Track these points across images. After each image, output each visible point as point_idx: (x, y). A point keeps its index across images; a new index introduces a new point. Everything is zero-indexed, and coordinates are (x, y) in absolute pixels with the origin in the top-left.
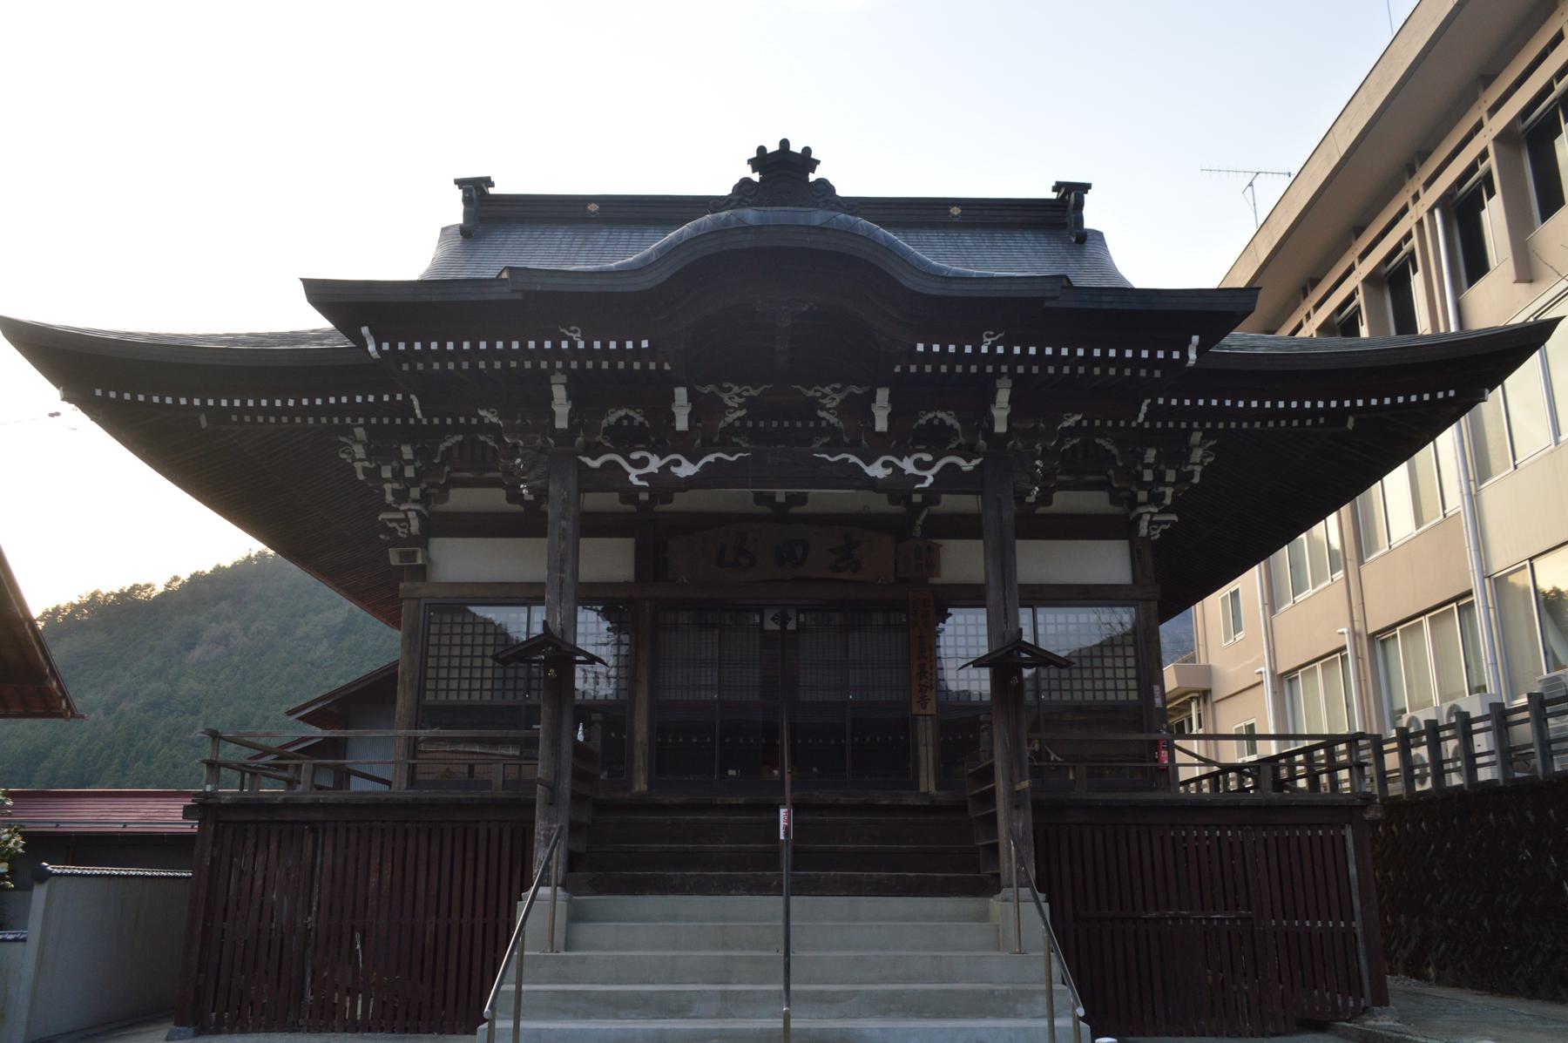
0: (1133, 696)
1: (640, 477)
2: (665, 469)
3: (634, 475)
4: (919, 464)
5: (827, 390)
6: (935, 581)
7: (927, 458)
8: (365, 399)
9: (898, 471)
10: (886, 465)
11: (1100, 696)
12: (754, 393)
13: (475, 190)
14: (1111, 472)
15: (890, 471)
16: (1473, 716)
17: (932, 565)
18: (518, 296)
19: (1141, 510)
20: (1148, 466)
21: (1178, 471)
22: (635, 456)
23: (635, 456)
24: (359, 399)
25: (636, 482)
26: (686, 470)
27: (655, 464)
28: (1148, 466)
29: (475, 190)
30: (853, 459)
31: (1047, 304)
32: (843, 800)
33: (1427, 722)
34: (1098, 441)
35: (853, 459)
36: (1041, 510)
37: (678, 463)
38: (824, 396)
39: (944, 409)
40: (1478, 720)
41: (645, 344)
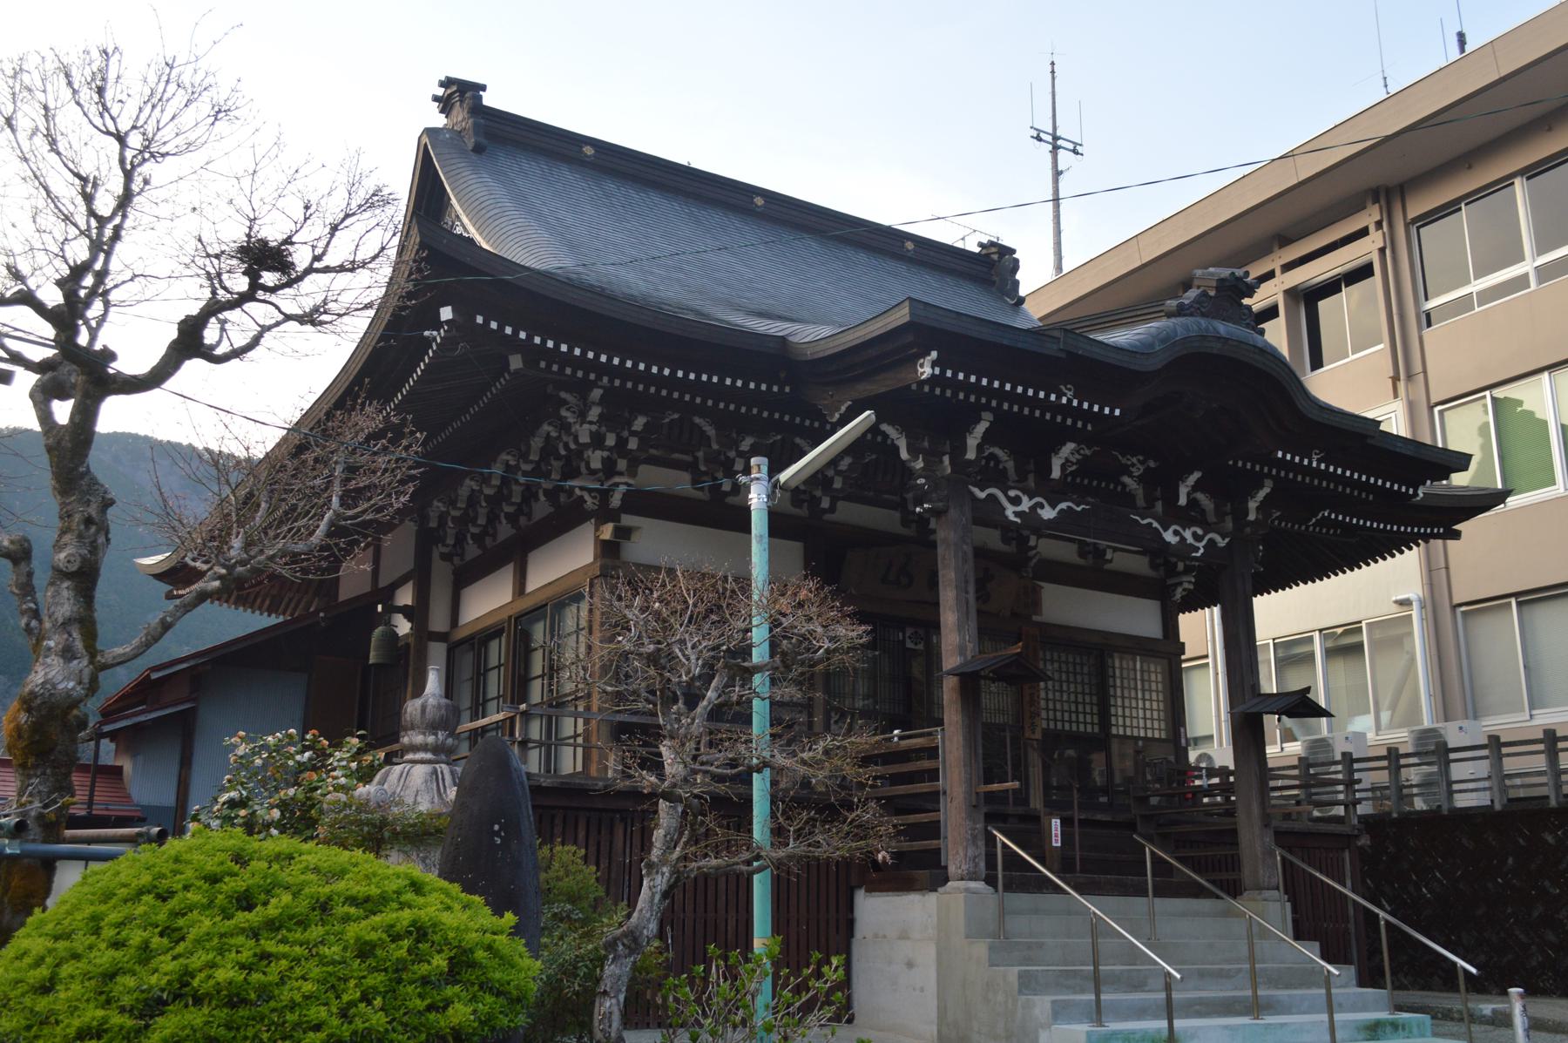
0: (1096, 729)
1: (1016, 514)
2: (1033, 508)
3: (1010, 511)
4: (1195, 535)
5: (1134, 460)
6: (1035, 618)
7: (1200, 532)
8: (710, 378)
9: (1183, 539)
10: (1176, 533)
11: (1074, 728)
12: (1088, 452)
13: (459, 93)
14: (700, 454)
15: (1177, 539)
16: (1401, 751)
17: (1036, 605)
18: (1063, 355)
19: (617, 479)
20: (634, 434)
21: (618, 436)
22: (1012, 493)
23: (1012, 493)
24: (739, 383)
25: (1012, 518)
26: (1048, 513)
27: (1026, 504)
28: (634, 434)
29: (459, 93)
30: (1156, 525)
31: (1369, 441)
32: (85, 846)
33: (1344, 754)
34: (697, 420)
35: (1156, 525)
36: (827, 517)
37: (1042, 507)
38: (1133, 465)
39: (1002, 448)
40: (1407, 755)
41: (1117, 412)
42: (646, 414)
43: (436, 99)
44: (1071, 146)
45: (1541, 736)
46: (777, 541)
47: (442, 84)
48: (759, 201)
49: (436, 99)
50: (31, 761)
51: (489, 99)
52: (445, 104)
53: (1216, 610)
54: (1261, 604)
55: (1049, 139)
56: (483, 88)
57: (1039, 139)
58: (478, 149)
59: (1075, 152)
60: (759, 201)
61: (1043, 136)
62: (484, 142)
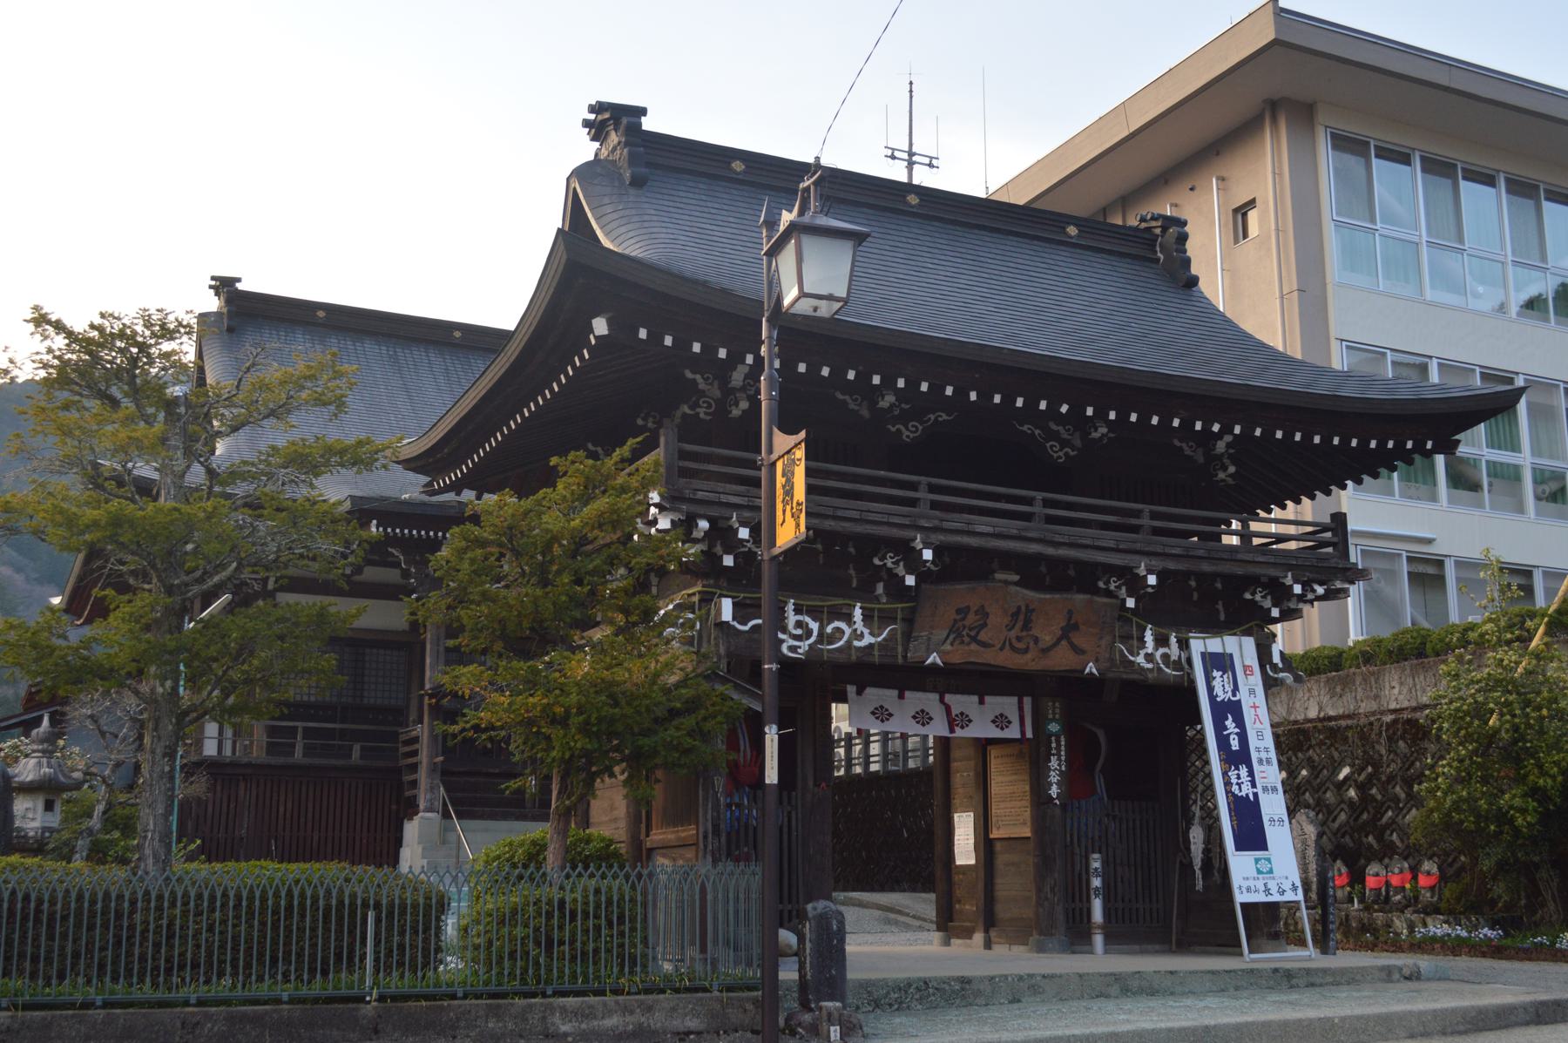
13: (612, 120)
29: (612, 120)
42: (791, 552)
43: (586, 123)
44: (927, 161)
45: (1327, 520)
46: (1429, 176)
47: (592, 109)
48: (321, 314)
49: (586, 123)
50: (1338, 689)
51: (648, 124)
52: (597, 130)
53: (973, 862)
54: (959, 862)
55: (905, 156)
56: (643, 111)
57: (893, 157)
58: (638, 182)
59: (930, 165)
60: (321, 314)
61: (897, 154)
62: (643, 170)
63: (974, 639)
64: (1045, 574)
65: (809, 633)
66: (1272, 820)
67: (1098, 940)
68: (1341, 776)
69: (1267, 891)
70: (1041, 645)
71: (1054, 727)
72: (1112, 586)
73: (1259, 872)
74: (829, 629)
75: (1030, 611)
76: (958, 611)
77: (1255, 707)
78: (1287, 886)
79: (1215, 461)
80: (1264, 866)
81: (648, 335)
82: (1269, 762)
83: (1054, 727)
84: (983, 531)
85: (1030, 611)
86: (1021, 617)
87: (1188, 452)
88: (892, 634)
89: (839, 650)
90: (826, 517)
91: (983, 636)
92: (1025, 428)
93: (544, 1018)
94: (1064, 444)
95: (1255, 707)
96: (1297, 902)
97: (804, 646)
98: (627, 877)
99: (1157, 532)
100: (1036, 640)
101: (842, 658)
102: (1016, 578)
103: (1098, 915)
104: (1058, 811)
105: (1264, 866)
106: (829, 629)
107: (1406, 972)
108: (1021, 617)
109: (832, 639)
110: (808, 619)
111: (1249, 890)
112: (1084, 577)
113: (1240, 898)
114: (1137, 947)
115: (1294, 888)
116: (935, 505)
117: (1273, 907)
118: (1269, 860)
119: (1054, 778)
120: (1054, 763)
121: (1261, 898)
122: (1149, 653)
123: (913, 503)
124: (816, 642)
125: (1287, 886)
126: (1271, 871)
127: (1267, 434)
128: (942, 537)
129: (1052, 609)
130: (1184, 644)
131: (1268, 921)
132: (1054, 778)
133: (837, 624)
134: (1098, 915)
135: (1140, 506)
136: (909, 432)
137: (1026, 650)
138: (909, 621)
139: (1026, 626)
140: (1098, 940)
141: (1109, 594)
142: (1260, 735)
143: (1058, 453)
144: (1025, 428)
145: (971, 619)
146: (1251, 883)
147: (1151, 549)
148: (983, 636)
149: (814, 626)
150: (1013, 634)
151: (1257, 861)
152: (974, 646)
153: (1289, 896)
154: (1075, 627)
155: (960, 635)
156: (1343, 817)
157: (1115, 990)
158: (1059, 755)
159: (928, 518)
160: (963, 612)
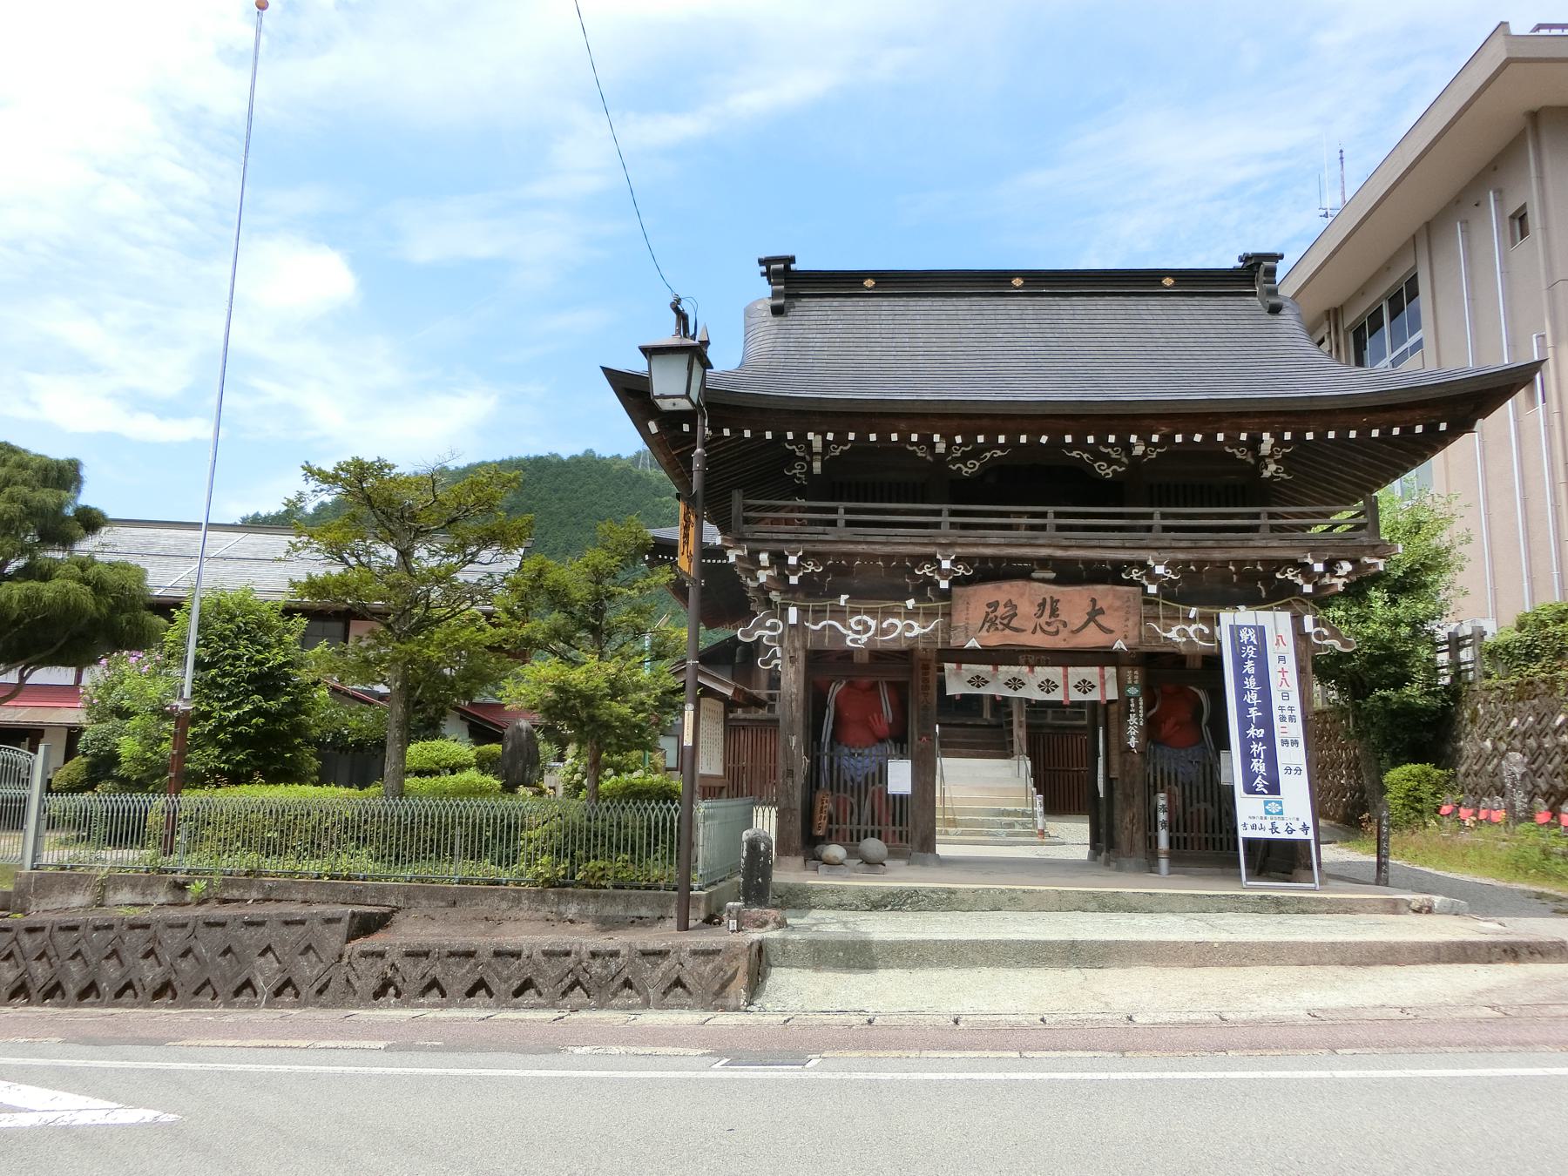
63: (1007, 626)
64: (1069, 574)
65: (867, 629)
66: (1288, 770)
67: (1164, 863)
68: (1558, 722)
69: (1274, 829)
70: (1070, 627)
71: (1133, 691)
72: (1134, 576)
73: (1267, 812)
74: (885, 625)
75: (1055, 602)
76: (989, 605)
77: (1283, 672)
78: (1297, 826)
79: (1261, 461)
80: (1273, 808)
81: (659, 426)
82: (1292, 719)
83: (1133, 691)
84: (993, 545)
85: (1055, 602)
86: (1048, 607)
87: (1239, 456)
88: (935, 630)
89: (893, 640)
90: (859, 543)
91: (1013, 624)
92: (1074, 454)
93: (1481, 856)
94: (1111, 462)
95: (1283, 672)
96: (1308, 841)
97: (864, 638)
98: (661, 809)
99: (1166, 529)
100: (1065, 625)
101: (895, 647)
102: (1052, 575)
103: (1163, 843)
104: (1137, 759)
105: (1273, 808)
106: (885, 625)
107: (1415, 906)
108: (1048, 607)
109: (884, 632)
110: (865, 618)
111: (1254, 827)
112: (1111, 574)
113: (1243, 833)
114: (1218, 870)
115: (1305, 828)
116: (953, 526)
117: (1292, 844)
118: (1280, 804)
119: (1132, 731)
120: (1132, 719)
121: (1267, 834)
122: (1181, 634)
123: (937, 525)
124: (875, 634)
125: (1297, 826)
126: (1281, 812)
127: (1320, 436)
128: (959, 550)
129: (1075, 600)
130: (1212, 621)
131: (1278, 860)
132: (1132, 731)
133: (891, 620)
134: (1163, 843)
135: (1150, 510)
136: (969, 469)
137: (1057, 633)
138: (948, 614)
139: (1054, 613)
140: (1164, 863)
141: (1131, 583)
142: (1286, 696)
143: (1105, 471)
144: (1074, 454)
145: (1001, 610)
146: (1258, 822)
147: (1159, 544)
148: (1013, 624)
149: (872, 623)
150: (1042, 620)
151: (1266, 803)
152: (1007, 631)
153: (1298, 835)
154: (1101, 611)
155: (993, 623)
156: (1558, 759)
157: (1094, 905)
158: (1137, 713)
159: (945, 536)
160: (994, 605)
